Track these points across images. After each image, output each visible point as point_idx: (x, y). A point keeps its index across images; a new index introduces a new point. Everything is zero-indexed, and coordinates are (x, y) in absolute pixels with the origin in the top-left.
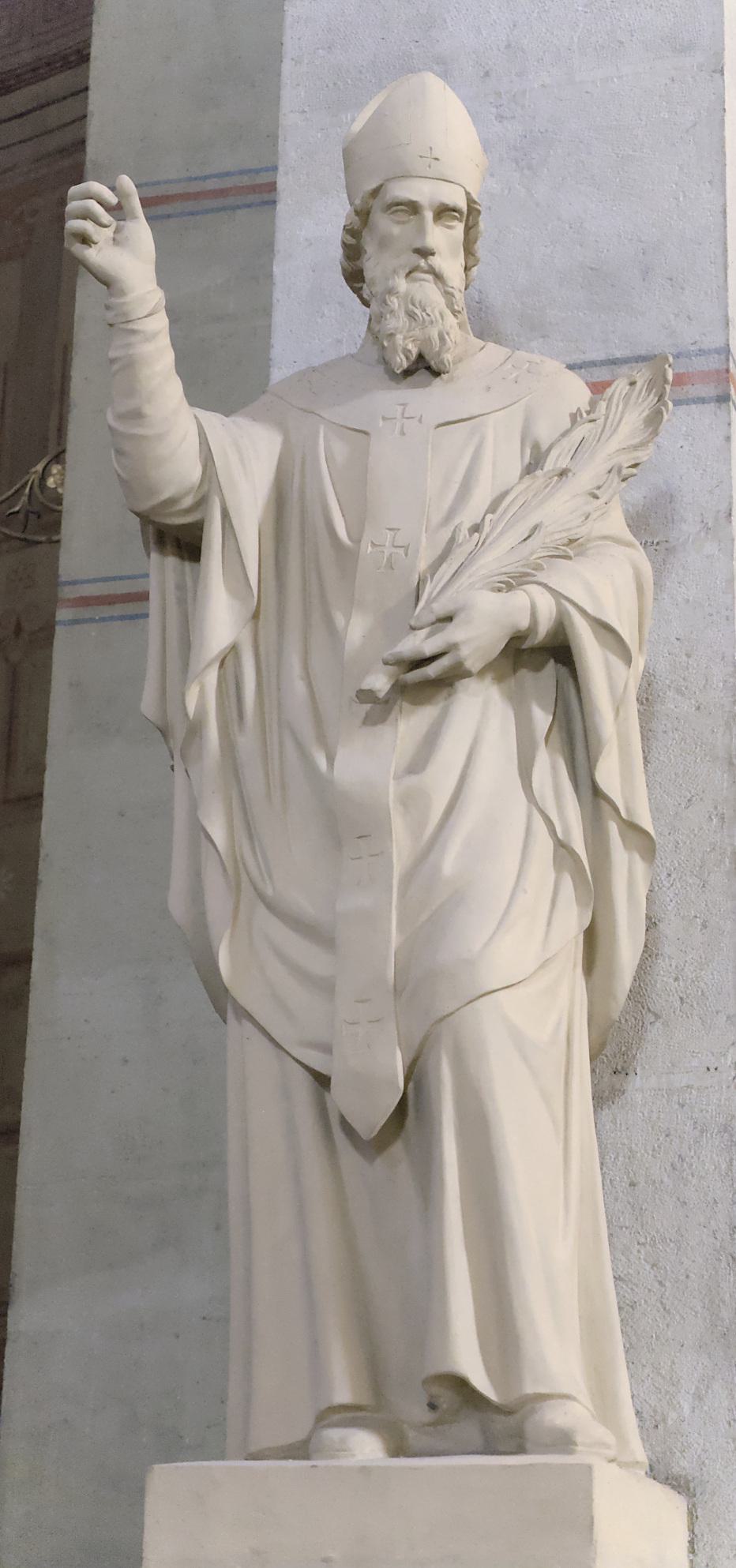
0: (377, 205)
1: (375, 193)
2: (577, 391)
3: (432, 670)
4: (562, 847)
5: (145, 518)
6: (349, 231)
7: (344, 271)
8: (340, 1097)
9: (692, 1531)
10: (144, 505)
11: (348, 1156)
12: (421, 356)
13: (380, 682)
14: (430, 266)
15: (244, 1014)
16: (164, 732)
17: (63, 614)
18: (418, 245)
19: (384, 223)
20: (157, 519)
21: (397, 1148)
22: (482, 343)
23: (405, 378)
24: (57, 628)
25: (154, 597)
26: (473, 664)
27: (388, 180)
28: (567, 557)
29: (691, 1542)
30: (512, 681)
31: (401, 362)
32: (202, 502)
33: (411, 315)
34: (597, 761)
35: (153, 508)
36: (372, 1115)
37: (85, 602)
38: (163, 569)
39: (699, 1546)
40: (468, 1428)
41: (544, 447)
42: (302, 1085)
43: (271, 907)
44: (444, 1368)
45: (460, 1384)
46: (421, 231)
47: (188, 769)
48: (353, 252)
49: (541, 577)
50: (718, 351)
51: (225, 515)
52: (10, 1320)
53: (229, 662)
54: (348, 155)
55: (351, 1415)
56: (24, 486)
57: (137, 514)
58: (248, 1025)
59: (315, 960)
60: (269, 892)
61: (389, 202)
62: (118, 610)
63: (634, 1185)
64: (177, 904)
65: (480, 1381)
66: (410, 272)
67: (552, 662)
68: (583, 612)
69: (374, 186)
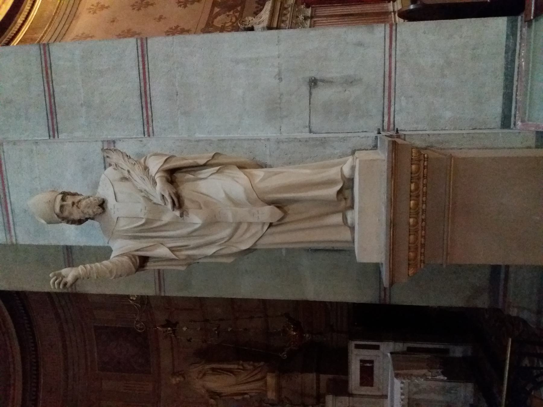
0: (61, 215)
1: (58, 216)
2: (110, 170)
3: (176, 200)
4: (218, 172)
5: (137, 270)
6: (68, 223)
7: (78, 225)
8: (274, 220)
9: (363, 150)
10: (134, 269)
11: (287, 220)
12: (99, 205)
13: (177, 213)
14: (77, 203)
15: (255, 244)
16: (189, 264)
17: (163, 294)
18: (71, 205)
19: (66, 214)
20: (137, 267)
21: (286, 208)
22: (97, 193)
23: (105, 210)
24: (166, 295)
25: (158, 268)
26: (174, 191)
27: (55, 212)
28: (149, 170)
29: (366, 150)
30: (179, 184)
31: (100, 210)
32: (134, 256)
33: (89, 207)
34: (199, 164)
35: (134, 265)
36: (278, 214)
37: (160, 290)
38: (150, 266)
39: (366, 148)
40: (347, 193)
41: (122, 176)
42: (273, 230)
43: (230, 239)
44: (335, 196)
45: (340, 192)
46: (67, 205)
47: (198, 258)
48: (73, 222)
49: (153, 175)
50: (103, 143)
51: (137, 250)
52: (312, 300)
53: (174, 249)
54: (49, 223)
55: (345, 218)
56: (135, 305)
57: (136, 272)
58: (258, 242)
59: (244, 226)
60: (228, 238)
61: (60, 212)
62: (162, 282)
63: (290, 163)
64: (230, 260)
65: (338, 187)
66: (78, 207)
67: (174, 174)
68: (162, 166)
69: (56, 216)
